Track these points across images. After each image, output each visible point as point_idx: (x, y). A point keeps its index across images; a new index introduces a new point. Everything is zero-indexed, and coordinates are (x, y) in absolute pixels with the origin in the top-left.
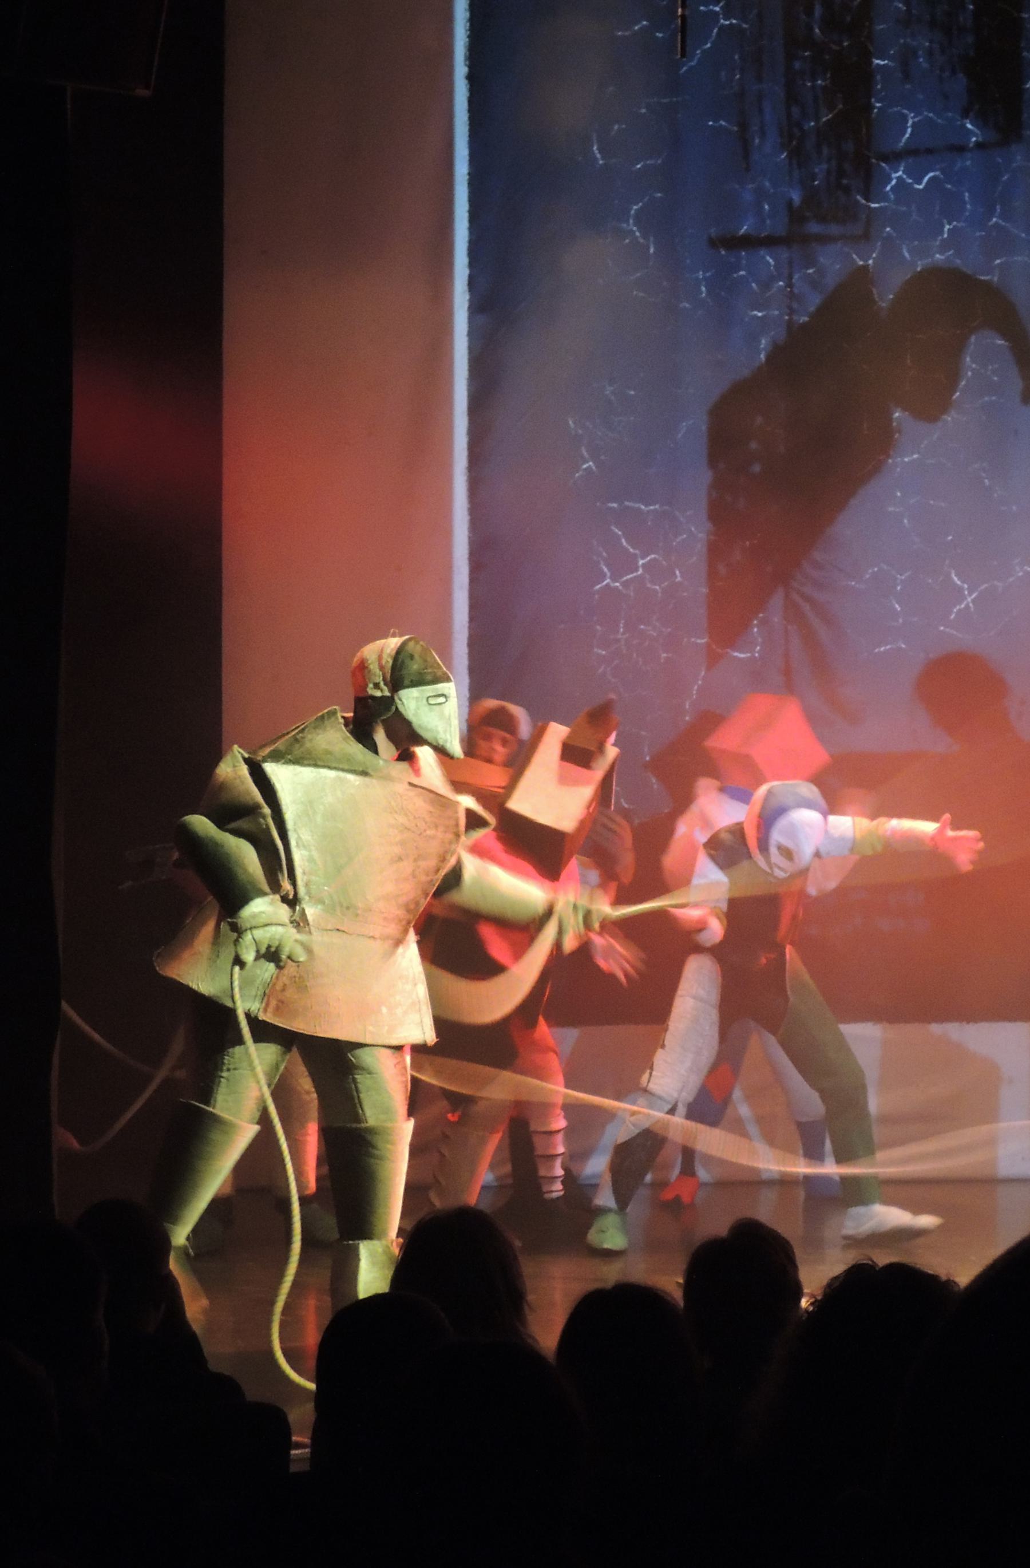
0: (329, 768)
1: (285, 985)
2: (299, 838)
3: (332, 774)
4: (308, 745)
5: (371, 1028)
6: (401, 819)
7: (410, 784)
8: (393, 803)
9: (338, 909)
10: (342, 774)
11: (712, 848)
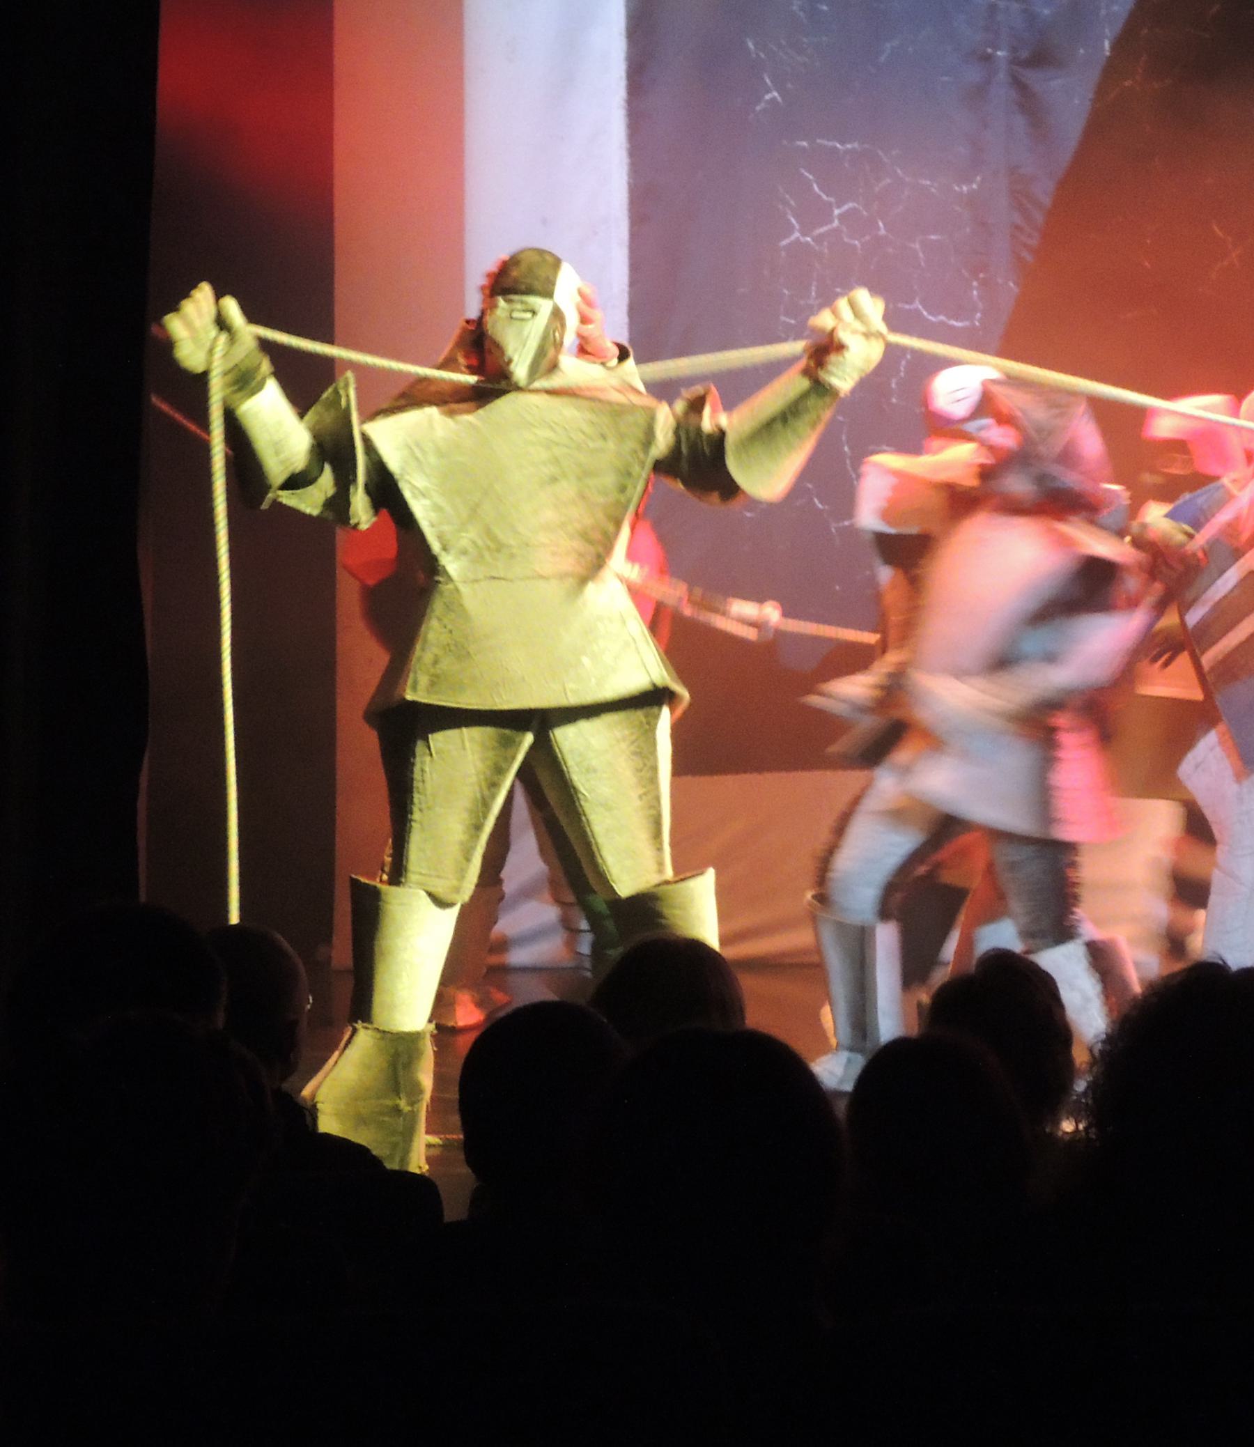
9: (487, 555)
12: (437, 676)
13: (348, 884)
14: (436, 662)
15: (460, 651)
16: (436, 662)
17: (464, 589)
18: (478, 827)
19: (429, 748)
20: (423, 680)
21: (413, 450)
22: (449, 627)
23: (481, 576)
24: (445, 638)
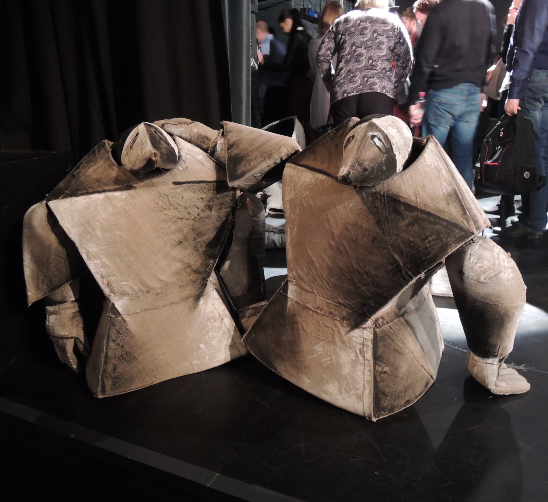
0: (99, 192)
1: (115, 365)
2: (88, 252)
3: (101, 196)
4: (82, 178)
5: (195, 362)
6: (173, 213)
7: (175, 183)
8: (160, 203)
9: (140, 294)
10: (109, 194)
11: (518, 363)
12: (117, 378)
13: (491, 241)
14: (115, 368)
15: (128, 357)
16: (115, 368)
17: (127, 319)
18: (459, 190)
19: (190, 141)
20: (109, 383)
21: (87, 225)
22: (121, 344)
23: (139, 310)
24: (119, 352)
